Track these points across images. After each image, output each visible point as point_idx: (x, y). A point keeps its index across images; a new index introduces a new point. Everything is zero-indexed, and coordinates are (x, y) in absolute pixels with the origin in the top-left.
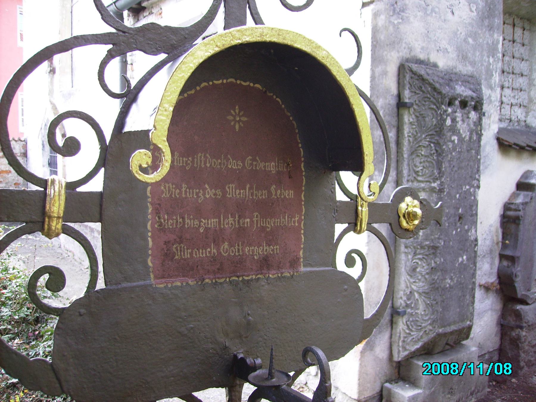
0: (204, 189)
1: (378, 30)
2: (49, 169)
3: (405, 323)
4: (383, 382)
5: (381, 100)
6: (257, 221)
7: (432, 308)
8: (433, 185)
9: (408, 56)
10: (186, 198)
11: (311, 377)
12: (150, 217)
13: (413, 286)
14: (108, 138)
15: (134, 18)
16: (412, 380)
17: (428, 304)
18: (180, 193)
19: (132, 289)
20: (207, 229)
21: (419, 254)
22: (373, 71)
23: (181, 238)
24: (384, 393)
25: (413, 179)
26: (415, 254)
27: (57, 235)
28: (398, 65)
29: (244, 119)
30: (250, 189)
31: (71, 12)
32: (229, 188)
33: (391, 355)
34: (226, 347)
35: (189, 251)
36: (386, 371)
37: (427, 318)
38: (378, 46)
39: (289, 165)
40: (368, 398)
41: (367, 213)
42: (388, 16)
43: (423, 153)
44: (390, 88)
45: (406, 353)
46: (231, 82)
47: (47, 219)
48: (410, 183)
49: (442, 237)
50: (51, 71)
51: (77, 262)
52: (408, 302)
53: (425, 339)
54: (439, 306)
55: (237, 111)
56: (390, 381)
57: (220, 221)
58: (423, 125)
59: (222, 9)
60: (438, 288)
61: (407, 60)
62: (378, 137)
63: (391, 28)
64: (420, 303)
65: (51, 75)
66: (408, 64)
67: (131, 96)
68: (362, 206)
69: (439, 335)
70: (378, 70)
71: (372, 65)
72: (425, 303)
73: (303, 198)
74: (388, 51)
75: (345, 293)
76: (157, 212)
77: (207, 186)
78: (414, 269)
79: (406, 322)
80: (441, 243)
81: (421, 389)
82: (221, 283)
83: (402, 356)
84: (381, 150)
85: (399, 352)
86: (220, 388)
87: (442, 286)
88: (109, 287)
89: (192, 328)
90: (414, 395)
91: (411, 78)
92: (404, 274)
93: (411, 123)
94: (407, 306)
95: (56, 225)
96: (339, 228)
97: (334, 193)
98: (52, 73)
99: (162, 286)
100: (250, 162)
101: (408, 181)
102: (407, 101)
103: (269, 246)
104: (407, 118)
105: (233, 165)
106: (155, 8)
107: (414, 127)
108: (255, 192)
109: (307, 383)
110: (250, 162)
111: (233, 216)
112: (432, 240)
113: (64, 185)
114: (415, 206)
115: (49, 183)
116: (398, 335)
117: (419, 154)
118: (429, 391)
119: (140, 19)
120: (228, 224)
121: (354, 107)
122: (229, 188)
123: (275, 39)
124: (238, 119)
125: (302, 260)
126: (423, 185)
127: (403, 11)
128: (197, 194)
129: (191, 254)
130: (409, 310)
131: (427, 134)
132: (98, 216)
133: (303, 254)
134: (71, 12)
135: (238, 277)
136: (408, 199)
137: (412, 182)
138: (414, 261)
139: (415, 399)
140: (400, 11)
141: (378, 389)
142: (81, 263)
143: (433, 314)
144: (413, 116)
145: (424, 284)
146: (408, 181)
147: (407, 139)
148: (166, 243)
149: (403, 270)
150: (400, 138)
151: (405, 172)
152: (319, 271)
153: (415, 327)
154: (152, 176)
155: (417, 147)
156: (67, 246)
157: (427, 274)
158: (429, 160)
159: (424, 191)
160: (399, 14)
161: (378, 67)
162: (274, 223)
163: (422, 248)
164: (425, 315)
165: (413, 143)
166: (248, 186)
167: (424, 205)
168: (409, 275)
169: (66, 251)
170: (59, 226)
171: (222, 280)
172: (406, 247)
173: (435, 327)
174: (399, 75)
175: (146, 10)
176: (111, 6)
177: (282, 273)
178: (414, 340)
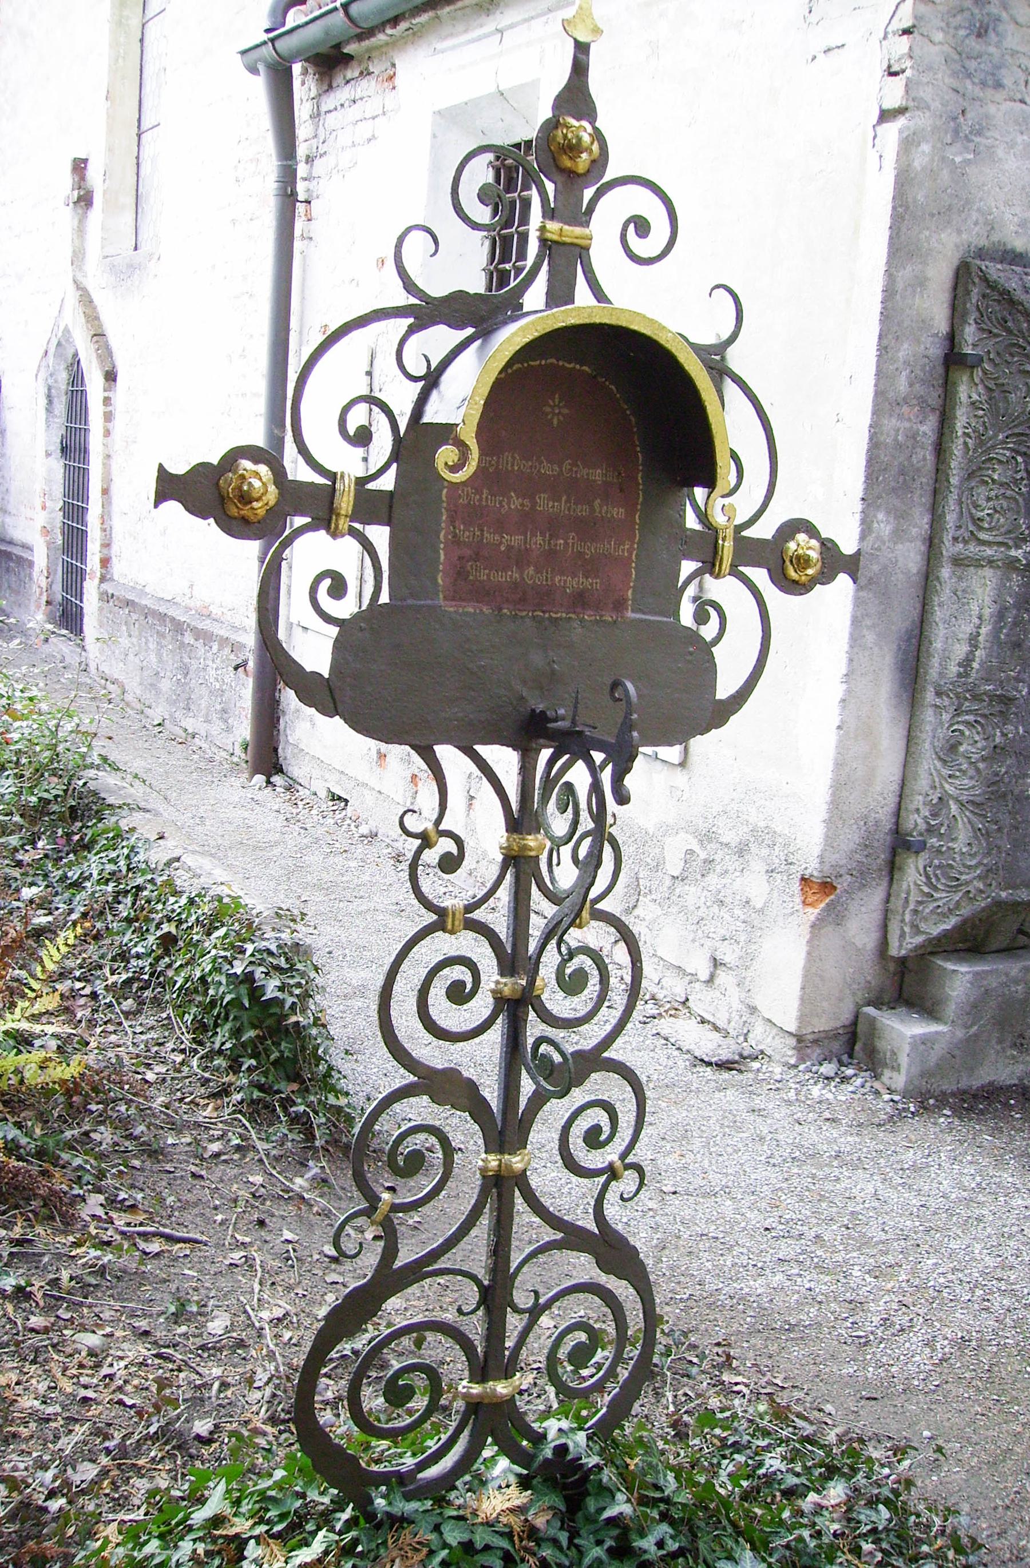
0: (509, 498)
1: (912, 179)
2: (62, 462)
3: (922, 872)
4: (861, 1002)
5: (906, 346)
6: (573, 544)
7: (987, 840)
8: (1013, 553)
9: (983, 242)
10: (487, 506)
11: (697, 985)
12: (443, 525)
13: (947, 786)
14: (402, 429)
15: (320, 80)
16: (928, 1004)
17: (979, 829)
18: (480, 500)
19: (418, 609)
20: (510, 548)
21: (968, 712)
22: (890, 275)
23: (477, 554)
24: (861, 1028)
25: (967, 535)
26: (958, 712)
27: (343, 536)
28: (956, 262)
29: (566, 411)
30: (566, 502)
31: (142, 40)
32: (540, 498)
33: (884, 943)
34: (523, 698)
35: (487, 571)
36: (869, 978)
37: (973, 863)
38: (907, 217)
39: (620, 474)
40: (822, 1035)
41: (732, 549)
42: (939, 145)
43: (996, 477)
44: (932, 319)
45: (919, 939)
46: (552, 364)
47: (334, 517)
48: (961, 545)
49: (1026, 676)
50: (80, 199)
51: (132, 709)
52: (933, 823)
53: (966, 911)
54: (1005, 837)
55: (557, 401)
56: (877, 1003)
57: (526, 539)
58: (1002, 411)
59: (545, 267)
60: (1004, 795)
61: (981, 253)
62: (893, 433)
63: (945, 174)
64: (960, 825)
65: (80, 211)
66: (978, 262)
67: (432, 379)
68: (724, 540)
69: (998, 904)
70: (905, 274)
71: (888, 263)
72: (972, 827)
73: (638, 521)
74: (933, 228)
75: (689, 658)
76: (452, 520)
77: (513, 494)
78: (953, 748)
79: (925, 867)
80: (1020, 692)
81: (946, 1023)
82: (522, 617)
83: (910, 946)
84: (896, 463)
85: (903, 935)
86: (510, 749)
87: (1016, 792)
88: (393, 602)
89: (483, 666)
90: (924, 1034)
91: (984, 296)
92: (928, 755)
93: (973, 403)
94: (930, 830)
95: (343, 524)
96: (688, 567)
97: (683, 517)
98: (83, 204)
99: (452, 609)
100: (569, 467)
101: (955, 539)
102: (968, 350)
103: (587, 578)
104: (966, 391)
105: (547, 469)
106: (376, 61)
107: (981, 413)
108: (573, 506)
109: (687, 1000)
110: (569, 467)
111: (543, 534)
112: (1001, 682)
113: (353, 479)
114: (810, 548)
115: (339, 477)
116: (904, 895)
117: (986, 479)
118: (964, 1031)
119: (334, 85)
120: (536, 543)
121: (706, 403)
122: (540, 498)
123: (606, 320)
124: (557, 411)
125: (630, 602)
126: (989, 552)
127: (979, 133)
128: (500, 503)
129: (488, 575)
130: (933, 841)
131: (1010, 432)
132: (386, 520)
133: (632, 594)
134: (142, 40)
135: (543, 612)
136: (801, 537)
137: (965, 542)
138: (955, 727)
139: (929, 1045)
140: (971, 133)
141: (846, 1017)
142: (142, 712)
143: (989, 854)
144: (980, 388)
145: (973, 783)
146: (955, 539)
147: (961, 441)
148: (461, 558)
149: (927, 746)
150: (945, 439)
151: (951, 518)
152: (653, 622)
153: (943, 881)
154: (457, 475)
155: (983, 462)
156: (104, 668)
157: (983, 759)
158: (1009, 493)
159: (991, 567)
160: (970, 141)
161: (905, 269)
162: (596, 549)
163: (976, 698)
164: (970, 855)
165: (975, 450)
166: (564, 498)
167: (829, 549)
168: (940, 759)
169: (103, 682)
170: (346, 527)
171: (524, 614)
172: (939, 694)
173: (990, 885)
174: (955, 288)
175: (354, 63)
176: (264, 48)
177: (601, 616)
178: (939, 911)
